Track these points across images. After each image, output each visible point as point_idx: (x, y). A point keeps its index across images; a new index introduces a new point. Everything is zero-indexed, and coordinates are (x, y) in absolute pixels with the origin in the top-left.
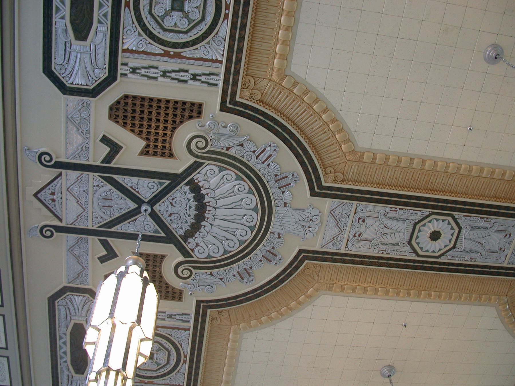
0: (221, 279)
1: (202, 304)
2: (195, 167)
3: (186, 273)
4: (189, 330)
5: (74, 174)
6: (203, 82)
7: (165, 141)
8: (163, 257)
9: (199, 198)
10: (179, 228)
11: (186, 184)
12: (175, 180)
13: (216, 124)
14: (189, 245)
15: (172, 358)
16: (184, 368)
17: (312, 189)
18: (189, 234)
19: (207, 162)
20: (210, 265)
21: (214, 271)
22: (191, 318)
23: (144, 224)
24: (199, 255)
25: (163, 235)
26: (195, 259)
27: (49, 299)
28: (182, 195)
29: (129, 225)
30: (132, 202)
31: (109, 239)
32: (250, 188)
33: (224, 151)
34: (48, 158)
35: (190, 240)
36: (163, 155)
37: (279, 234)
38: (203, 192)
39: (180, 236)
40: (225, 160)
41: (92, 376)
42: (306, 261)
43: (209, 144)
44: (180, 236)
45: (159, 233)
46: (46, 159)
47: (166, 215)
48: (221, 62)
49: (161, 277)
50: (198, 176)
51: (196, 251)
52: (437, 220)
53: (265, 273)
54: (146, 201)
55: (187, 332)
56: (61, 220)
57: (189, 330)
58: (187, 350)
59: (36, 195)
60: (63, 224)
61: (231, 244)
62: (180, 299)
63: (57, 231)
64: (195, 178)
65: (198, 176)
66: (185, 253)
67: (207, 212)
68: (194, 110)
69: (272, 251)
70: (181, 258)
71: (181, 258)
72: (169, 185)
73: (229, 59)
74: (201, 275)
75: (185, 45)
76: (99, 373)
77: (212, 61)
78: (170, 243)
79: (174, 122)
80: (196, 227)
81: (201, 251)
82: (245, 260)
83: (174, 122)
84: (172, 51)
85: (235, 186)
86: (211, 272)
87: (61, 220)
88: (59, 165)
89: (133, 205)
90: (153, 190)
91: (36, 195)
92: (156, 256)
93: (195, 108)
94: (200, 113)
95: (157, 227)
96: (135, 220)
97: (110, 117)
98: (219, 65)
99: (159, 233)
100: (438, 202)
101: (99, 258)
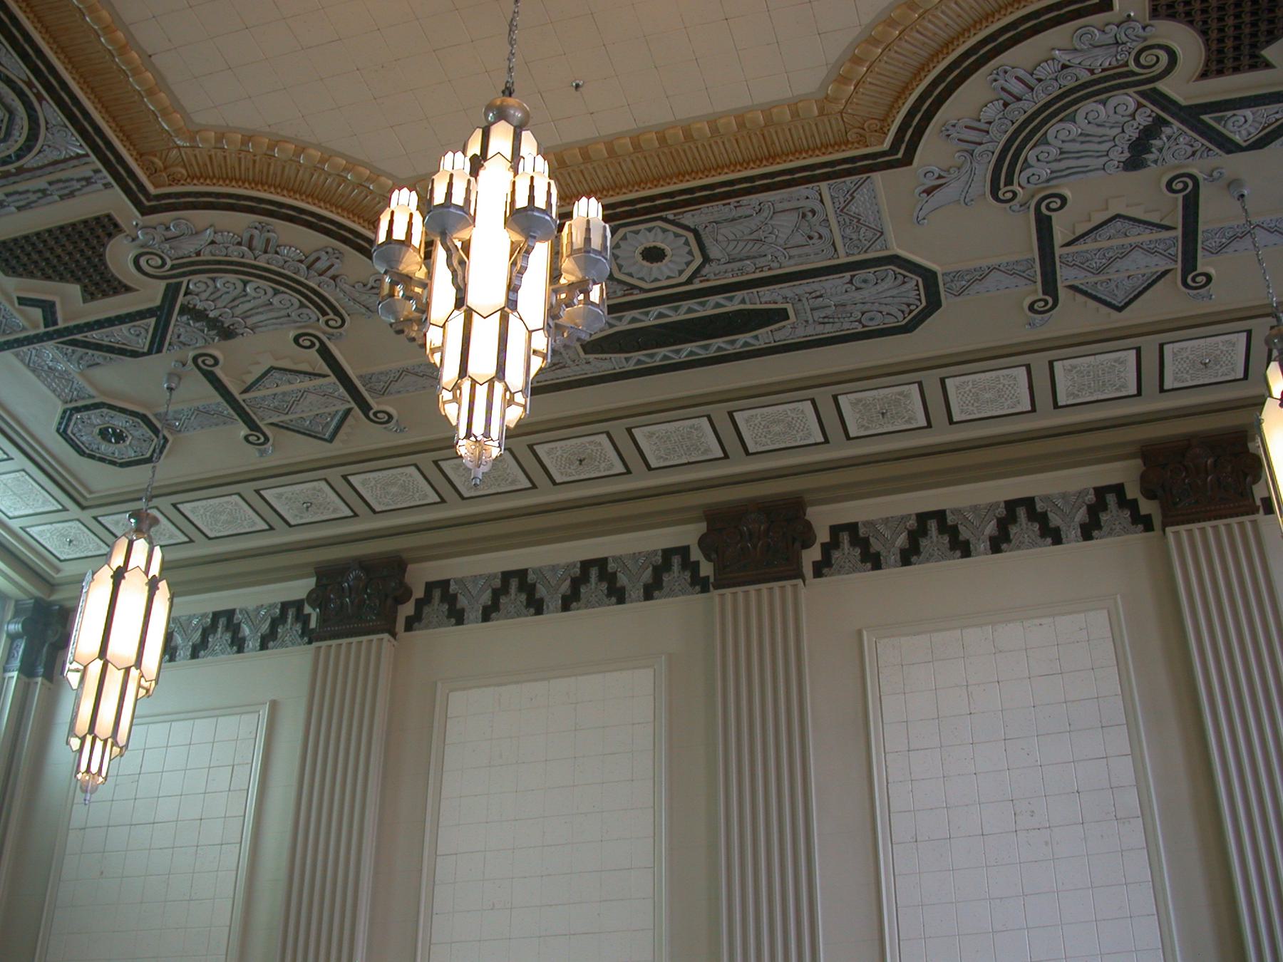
3: (1149, 58)
8: (1204, 75)
14: (1149, 112)
17: (137, 203)
18: (1150, 132)
20: (1100, 86)
24: (1127, 100)
25: (1205, 118)
26: (1131, 91)
30: (1272, 145)
39: (1167, 123)
41: (447, 395)
42: (886, 146)
45: (1215, 119)
49: (1204, 33)
52: (664, 231)
61: (1062, 135)
70: (1161, 86)
75: (20, 155)
76: (457, 387)
78: (1190, 107)
81: (1121, 109)
92: (1220, 72)
95: (1219, 128)
96: (1264, 128)
97: (109, 216)
98: (87, 159)
100: (26, 41)
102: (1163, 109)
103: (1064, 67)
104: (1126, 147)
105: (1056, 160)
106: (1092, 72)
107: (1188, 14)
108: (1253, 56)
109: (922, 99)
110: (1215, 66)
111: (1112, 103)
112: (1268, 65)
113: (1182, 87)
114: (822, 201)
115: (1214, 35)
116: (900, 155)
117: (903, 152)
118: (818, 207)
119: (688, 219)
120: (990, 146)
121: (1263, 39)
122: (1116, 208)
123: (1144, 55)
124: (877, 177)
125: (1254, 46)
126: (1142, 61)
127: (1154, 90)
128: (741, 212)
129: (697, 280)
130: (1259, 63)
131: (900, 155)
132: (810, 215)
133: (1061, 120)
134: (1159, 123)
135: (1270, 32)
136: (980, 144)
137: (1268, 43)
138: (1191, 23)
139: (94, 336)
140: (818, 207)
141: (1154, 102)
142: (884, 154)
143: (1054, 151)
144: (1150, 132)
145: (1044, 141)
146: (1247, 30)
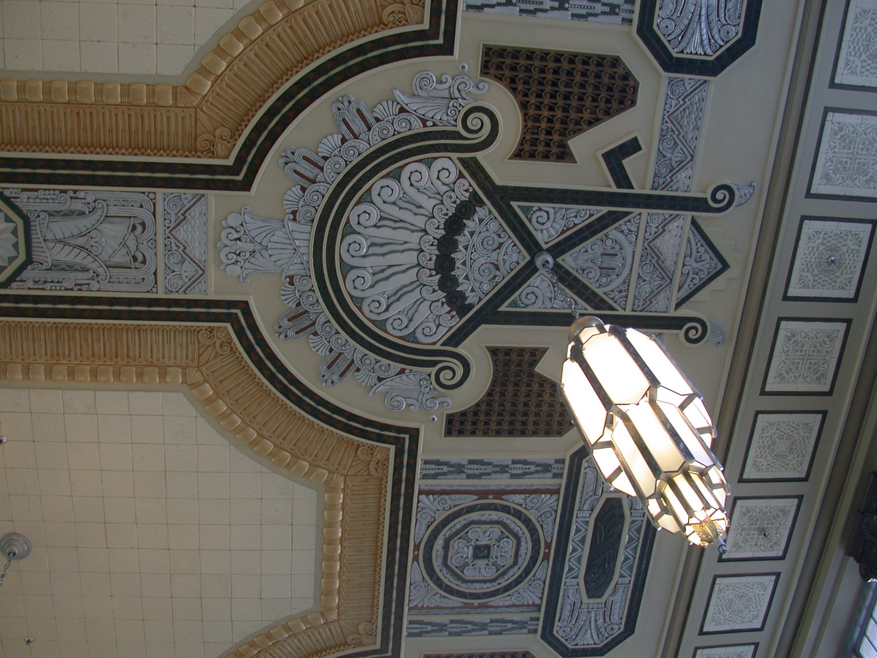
2: (457, 338)
4: (410, 609)
9: (448, 283)
11: (471, 306)
12: (490, 314)
14: (467, 186)
16: (418, 532)
18: (465, 210)
19: (438, 347)
20: (425, 144)
23: (548, 224)
24: (448, 165)
26: (455, 156)
28: (476, 287)
32: (360, 309)
34: (692, 334)
37: (294, 219)
39: (482, 204)
40: (407, 354)
42: (230, 162)
43: (433, 376)
45: (510, 305)
58: (415, 572)
59: (725, 266)
60: (689, 215)
66: (475, 169)
67: (434, 258)
68: (457, 425)
72: (502, 302)
74: (443, 118)
86: (425, 126)
87: (694, 222)
89: (568, 260)
91: (725, 266)
93: (457, 426)
96: (563, 232)
99: (510, 305)
102: (477, 313)
103: (402, 110)
104: (443, 221)
105: (375, 226)
106: (424, 122)
107: (513, 81)
108: (563, 146)
111: (437, 165)
113: (503, 167)
114: (154, 214)
116: (240, 178)
117: (240, 176)
118: (148, 219)
119: (25, 201)
124: (211, 194)
127: (475, 160)
128: (77, 206)
129: (14, 285)
130: (564, 155)
131: (240, 178)
132: (139, 228)
133: (383, 177)
135: (621, 102)
137: (576, 133)
138: (514, 90)
140: (148, 219)
141: (472, 175)
142: (225, 170)
143: (375, 215)
144: (465, 210)
145: (366, 199)
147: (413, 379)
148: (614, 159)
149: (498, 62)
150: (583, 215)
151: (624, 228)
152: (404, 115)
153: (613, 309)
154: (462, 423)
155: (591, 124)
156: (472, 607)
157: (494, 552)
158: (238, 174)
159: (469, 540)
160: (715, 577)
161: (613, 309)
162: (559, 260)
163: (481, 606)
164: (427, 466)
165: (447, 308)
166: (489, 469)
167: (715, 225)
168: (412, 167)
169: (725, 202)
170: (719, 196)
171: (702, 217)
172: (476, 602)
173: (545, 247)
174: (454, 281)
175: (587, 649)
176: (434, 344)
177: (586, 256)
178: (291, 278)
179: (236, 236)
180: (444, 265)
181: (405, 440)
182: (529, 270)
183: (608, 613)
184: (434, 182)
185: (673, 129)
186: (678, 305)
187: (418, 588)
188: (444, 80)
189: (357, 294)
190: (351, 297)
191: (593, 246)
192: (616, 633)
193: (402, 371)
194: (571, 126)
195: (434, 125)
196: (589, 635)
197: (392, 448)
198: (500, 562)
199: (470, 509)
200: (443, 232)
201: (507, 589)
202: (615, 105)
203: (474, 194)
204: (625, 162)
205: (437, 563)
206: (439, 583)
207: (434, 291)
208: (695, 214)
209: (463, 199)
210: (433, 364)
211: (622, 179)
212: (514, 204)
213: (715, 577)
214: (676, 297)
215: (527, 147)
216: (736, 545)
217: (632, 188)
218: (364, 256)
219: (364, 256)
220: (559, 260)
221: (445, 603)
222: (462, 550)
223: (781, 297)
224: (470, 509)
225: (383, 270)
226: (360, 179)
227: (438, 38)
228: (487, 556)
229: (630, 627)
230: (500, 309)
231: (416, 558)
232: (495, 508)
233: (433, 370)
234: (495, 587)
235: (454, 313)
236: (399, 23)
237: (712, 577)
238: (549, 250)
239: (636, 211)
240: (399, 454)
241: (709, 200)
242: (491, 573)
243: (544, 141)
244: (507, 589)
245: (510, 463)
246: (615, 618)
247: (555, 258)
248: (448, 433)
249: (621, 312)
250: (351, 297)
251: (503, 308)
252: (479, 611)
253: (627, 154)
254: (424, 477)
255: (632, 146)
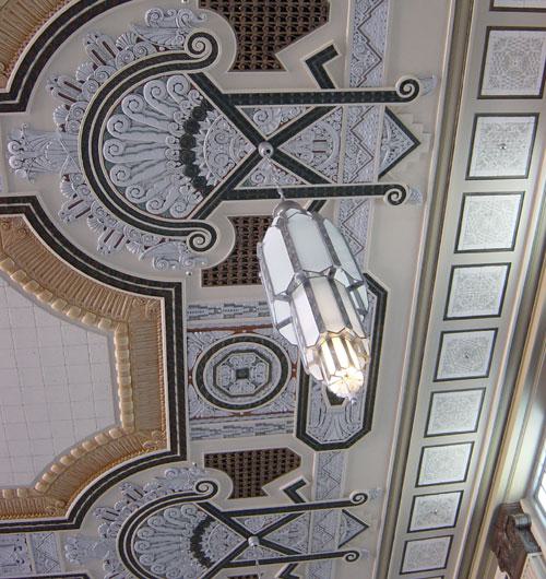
0: (139, 40)
1: (179, 454)
2: (206, 211)
4: (190, 420)
5: (328, 549)
6: (206, 307)
7: (245, 238)
9: (192, 171)
10: (217, 120)
11: (212, 188)
12: (228, 192)
13: (179, 263)
15: (211, 378)
16: (191, 362)
18: (200, 113)
19: (189, 220)
21: (154, 54)
22: (191, 434)
23: (267, 121)
24: (183, 78)
25: (238, 188)
27: (370, 429)
28: (215, 175)
29: (290, 117)
31: (294, 504)
32: (124, 195)
33: (167, 238)
34: (394, 197)
35: (197, 104)
36: (246, 220)
37: (64, 131)
38: (188, 115)
39: (211, 109)
40: (166, 228)
42: (67, 516)
43: (188, 243)
44: (214, 520)
45: (244, 185)
46: (395, 195)
47: (231, 534)
48: (189, 331)
50: (199, 201)
51: (186, 86)
53: (115, 497)
54: (267, 139)
55: (192, 416)
56: (343, 511)
57: (190, 420)
58: (191, 392)
59: (417, 143)
60: (382, 106)
62: (207, 457)
63: (349, 502)
64: (201, 198)
65: (199, 201)
66: (202, 81)
67: (178, 152)
68: (212, 277)
69: (68, 102)
70: (209, 501)
71: (209, 501)
72: (236, 183)
73: (180, 335)
74: (176, 43)
77: (198, 331)
79: (235, 261)
80: (192, 126)
82: (107, 81)
83: (235, 261)
84: (244, 334)
85: (145, 195)
86: (158, 51)
87: (387, 111)
88: (378, 190)
89: (285, 148)
90: (259, 172)
91: (417, 143)
93: (211, 278)
94: (205, 276)
96: (280, 126)
99: (244, 185)
101: (305, 484)
106: (157, 48)
107: (226, 9)
109: (34, 49)
110: (243, 63)
112: (265, 495)
113: (222, 502)
115: (237, 478)
116: (17, 101)
120: (81, 105)
121: (277, 42)
122: (170, 142)
123: (195, 41)
125: (270, 49)
126: (200, 487)
127: (201, 75)
130: (273, 66)
131: (17, 101)
134: (208, 521)
135: (282, 39)
136: (75, 101)
137: (280, 47)
138: (226, 471)
139: (282, 516)
142: (65, 521)
143: (151, 532)
144: (200, 113)
146: (253, 482)
147: (177, 246)
148: (316, 64)
149: (213, 461)
150: (295, 112)
151: (329, 119)
152: (141, 44)
153: (328, 183)
154: (215, 276)
155: (293, 39)
156: (238, 415)
157: (252, 373)
158: (14, 99)
159: (231, 366)
160: (453, 268)
161: (328, 183)
162: (279, 148)
163: (246, 414)
164: (192, 310)
165: (193, 190)
166: (241, 310)
167: (407, 112)
168: (149, 85)
169: (412, 93)
170: (406, 88)
171: (392, 105)
172: (242, 412)
173: (267, 139)
174: (203, 553)
175: (361, 187)
176: (185, 218)
177: (302, 144)
178: (67, 176)
179: (19, 147)
180: (187, 143)
181: (171, 293)
182: (255, 158)
183: (348, 416)
184: (173, 95)
185: (323, 472)
186: (340, 547)
187: (196, 405)
188: (170, 14)
189: (119, 184)
190: (116, 187)
191: (307, 134)
192: (357, 430)
193: (163, 240)
194: (277, 42)
195: (166, 49)
196: (334, 433)
197: (162, 300)
198: (259, 380)
199: (229, 342)
200: (183, 132)
201: (263, 401)
202: (311, 21)
203: (204, 102)
204: (324, 65)
205: (208, 384)
206: (210, 398)
207: (181, 178)
208: (388, 104)
209: (196, 105)
210: (187, 233)
211: (324, 81)
212: (239, 108)
213: (443, 333)
214: (337, 543)
215: (242, 61)
216: (419, 523)
217: (334, 88)
218: (122, 155)
219: (122, 155)
220: (279, 148)
221: (218, 414)
222: (226, 374)
223: (476, 96)
224: (229, 342)
225: (135, 145)
226: (111, 97)
227: (171, 292)
228: (247, 377)
229: (367, 426)
230: (237, 107)
231: (190, 382)
232: (248, 340)
233: (188, 238)
234: (255, 400)
235: (198, 193)
236: (152, 447)
237: (450, 268)
238: (269, 141)
239: (339, 105)
240: (168, 304)
241: (399, 93)
242: (252, 389)
243: (258, 53)
244: (263, 401)
245: (257, 304)
246: (355, 420)
247: (275, 147)
248: (205, 283)
249: (333, 184)
250: (116, 187)
251: (238, 188)
252: (245, 418)
253: (298, 488)
254: (190, 319)
255: (330, 53)
